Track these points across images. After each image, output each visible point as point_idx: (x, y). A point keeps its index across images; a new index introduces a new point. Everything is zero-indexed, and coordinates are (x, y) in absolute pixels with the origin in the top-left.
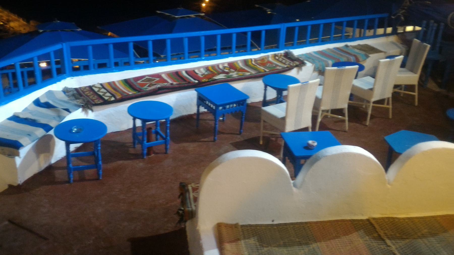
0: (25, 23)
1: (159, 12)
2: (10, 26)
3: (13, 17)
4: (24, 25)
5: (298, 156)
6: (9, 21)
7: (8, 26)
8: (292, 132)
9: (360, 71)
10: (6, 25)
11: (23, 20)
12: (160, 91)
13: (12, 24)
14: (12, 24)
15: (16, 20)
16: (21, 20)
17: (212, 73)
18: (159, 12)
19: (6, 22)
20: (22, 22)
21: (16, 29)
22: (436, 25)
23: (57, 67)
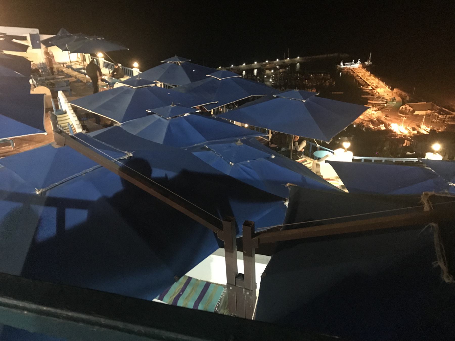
0: (389, 90)
1: (208, 76)
2: (377, 91)
3: (382, 84)
4: (389, 92)
5: (103, 54)
6: (377, 87)
7: (375, 91)
8: (215, 285)
9: (439, 153)
10: (374, 90)
11: (388, 87)
12: (84, 59)
13: (379, 90)
14: (379, 90)
15: (383, 87)
16: (387, 87)
17: (398, 157)
18: (208, 76)
19: (375, 88)
20: (387, 89)
21: (380, 94)
22: (385, 102)
23: (362, 160)
